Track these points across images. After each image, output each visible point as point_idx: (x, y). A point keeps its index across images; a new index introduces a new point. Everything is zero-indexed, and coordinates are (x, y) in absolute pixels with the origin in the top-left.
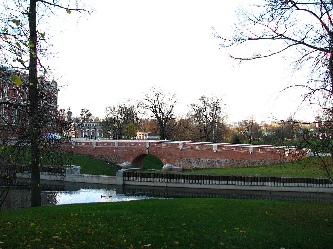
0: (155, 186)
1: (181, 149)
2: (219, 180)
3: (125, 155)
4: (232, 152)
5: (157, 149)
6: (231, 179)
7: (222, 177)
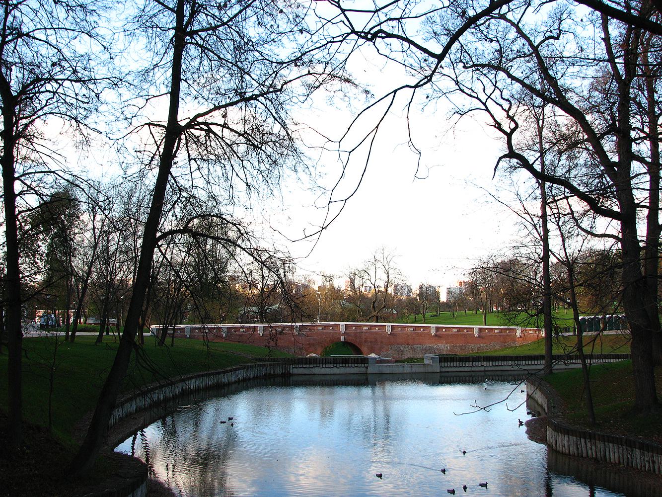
0: (473, 371)
1: (389, 333)
2: (538, 360)
3: (309, 344)
4: (453, 336)
5: (355, 334)
6: (471, 359)
7: (528, 356)
